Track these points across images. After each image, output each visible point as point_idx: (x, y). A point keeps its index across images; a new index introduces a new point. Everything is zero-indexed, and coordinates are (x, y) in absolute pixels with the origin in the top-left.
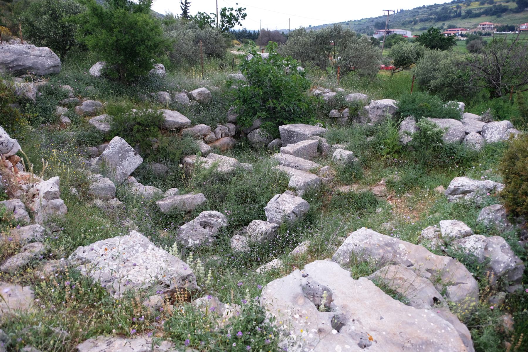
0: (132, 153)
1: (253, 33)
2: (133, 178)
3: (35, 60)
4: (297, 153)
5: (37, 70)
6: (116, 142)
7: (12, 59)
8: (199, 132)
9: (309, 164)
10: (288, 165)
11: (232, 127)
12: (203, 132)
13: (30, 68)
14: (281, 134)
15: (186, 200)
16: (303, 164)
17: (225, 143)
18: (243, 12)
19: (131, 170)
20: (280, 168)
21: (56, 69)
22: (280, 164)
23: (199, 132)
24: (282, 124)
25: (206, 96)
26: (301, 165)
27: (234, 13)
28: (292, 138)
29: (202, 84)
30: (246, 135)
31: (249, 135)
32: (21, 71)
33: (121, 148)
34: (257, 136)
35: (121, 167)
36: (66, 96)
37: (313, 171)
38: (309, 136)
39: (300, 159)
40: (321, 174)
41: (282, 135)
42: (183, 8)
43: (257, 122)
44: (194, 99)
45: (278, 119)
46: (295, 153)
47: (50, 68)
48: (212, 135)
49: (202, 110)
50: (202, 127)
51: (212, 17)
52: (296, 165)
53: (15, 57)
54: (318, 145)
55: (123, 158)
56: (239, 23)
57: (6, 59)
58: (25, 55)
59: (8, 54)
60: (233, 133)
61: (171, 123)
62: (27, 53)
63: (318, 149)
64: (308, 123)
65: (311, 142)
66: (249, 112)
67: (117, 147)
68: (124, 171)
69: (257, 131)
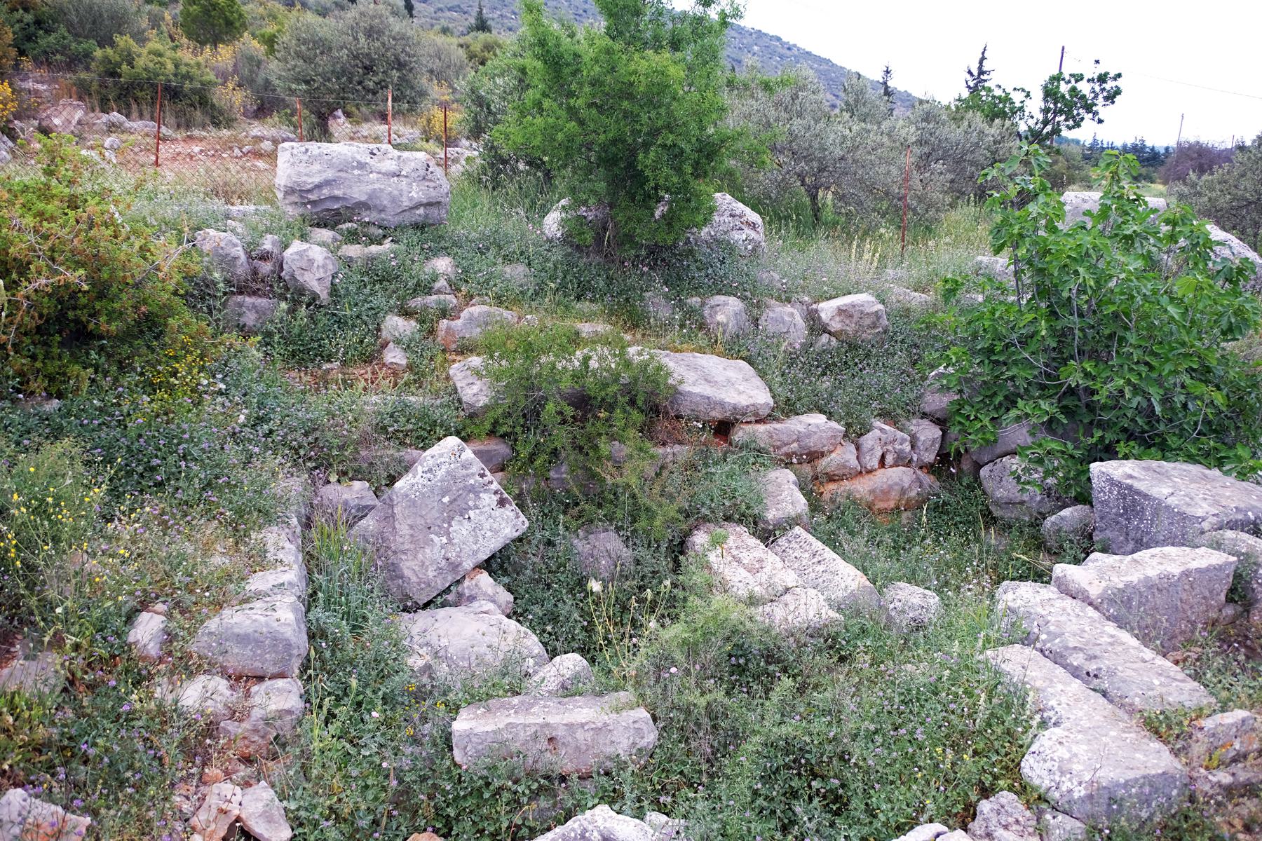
0: (489, 500)
1: (1162, 151)
2: (484, 579)
3: (376, 186)
4: (1121, 608)
5: (381, 211)
6: (441, 455)
7: (317, 180)
8: (798, 440)
9: (1162, 681)
10: (1057, 658)
11: (929, 433)
12: (813, 443)
13: (364, 206)
14: (1095, 494)
15: (560, 733)
16: (1125, 672)
17: (890, 487)
18: (1109, 85)
19: (475, 553)
20: (1016, 662)
21: (434, 212)
22: (1028, 640)
23: (798, 440)
24: (1108, 452)
25: (867, 321)
26: (1112, 673)
27: (1084, 88)
28: (1135, 525)
29: (862, 284)
30: (978, 466)
31: (984, 472)
32: (337, 212)
33: (454, 478)
34: (1007, 480)
35: (444, 540)
36: (424, 288)
37: (1163, 727)
38: (1206, 525)
39: (1125, 636)
40: (1198, 749)
41: (1097, 495)
42: (971, 84)
43: (1017, 434)
44: (825, 330)
45: (1098, 433)
46: (1112, 601)
47: (417, 207)
48: (845, 455)
49: (834, 368)
50: (814, 425)
51: (1017, 98)
52: (1092, 667)
53: (330, 174)
54: (1238, 576)
55: (458, 509)
56: (1096, 113)
57: (304, 178)
58: (356, 172)
59: (316, 167)
60: (930, 457)
61: (697, 404)
62: (361, 166)
63: (1232, 590)
64: (1220, 464)
65: (1205, 558)
66: (995, 394)
67: (441, 473)
68: (452, 555)
69: (1014, 463)
